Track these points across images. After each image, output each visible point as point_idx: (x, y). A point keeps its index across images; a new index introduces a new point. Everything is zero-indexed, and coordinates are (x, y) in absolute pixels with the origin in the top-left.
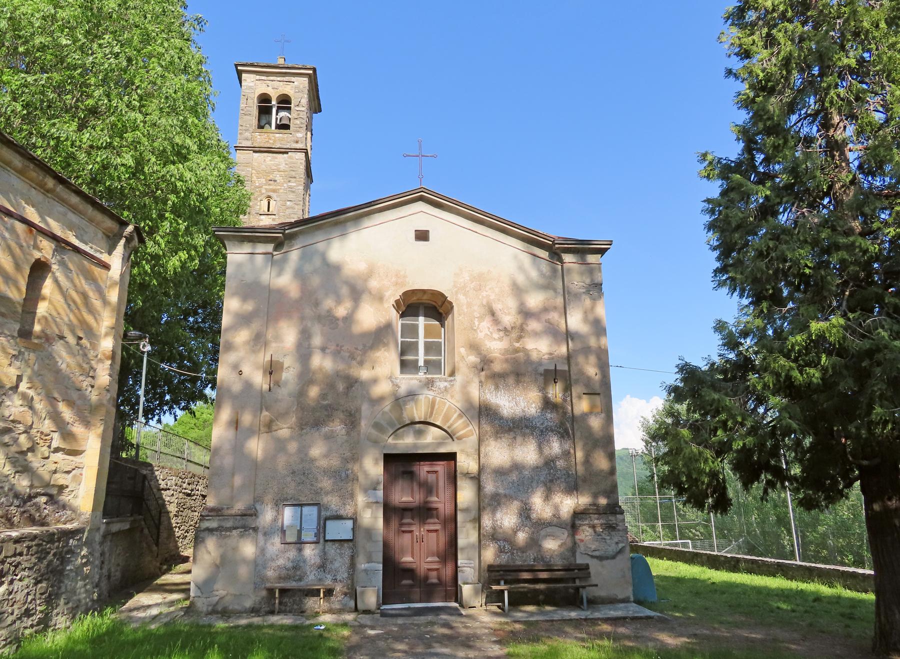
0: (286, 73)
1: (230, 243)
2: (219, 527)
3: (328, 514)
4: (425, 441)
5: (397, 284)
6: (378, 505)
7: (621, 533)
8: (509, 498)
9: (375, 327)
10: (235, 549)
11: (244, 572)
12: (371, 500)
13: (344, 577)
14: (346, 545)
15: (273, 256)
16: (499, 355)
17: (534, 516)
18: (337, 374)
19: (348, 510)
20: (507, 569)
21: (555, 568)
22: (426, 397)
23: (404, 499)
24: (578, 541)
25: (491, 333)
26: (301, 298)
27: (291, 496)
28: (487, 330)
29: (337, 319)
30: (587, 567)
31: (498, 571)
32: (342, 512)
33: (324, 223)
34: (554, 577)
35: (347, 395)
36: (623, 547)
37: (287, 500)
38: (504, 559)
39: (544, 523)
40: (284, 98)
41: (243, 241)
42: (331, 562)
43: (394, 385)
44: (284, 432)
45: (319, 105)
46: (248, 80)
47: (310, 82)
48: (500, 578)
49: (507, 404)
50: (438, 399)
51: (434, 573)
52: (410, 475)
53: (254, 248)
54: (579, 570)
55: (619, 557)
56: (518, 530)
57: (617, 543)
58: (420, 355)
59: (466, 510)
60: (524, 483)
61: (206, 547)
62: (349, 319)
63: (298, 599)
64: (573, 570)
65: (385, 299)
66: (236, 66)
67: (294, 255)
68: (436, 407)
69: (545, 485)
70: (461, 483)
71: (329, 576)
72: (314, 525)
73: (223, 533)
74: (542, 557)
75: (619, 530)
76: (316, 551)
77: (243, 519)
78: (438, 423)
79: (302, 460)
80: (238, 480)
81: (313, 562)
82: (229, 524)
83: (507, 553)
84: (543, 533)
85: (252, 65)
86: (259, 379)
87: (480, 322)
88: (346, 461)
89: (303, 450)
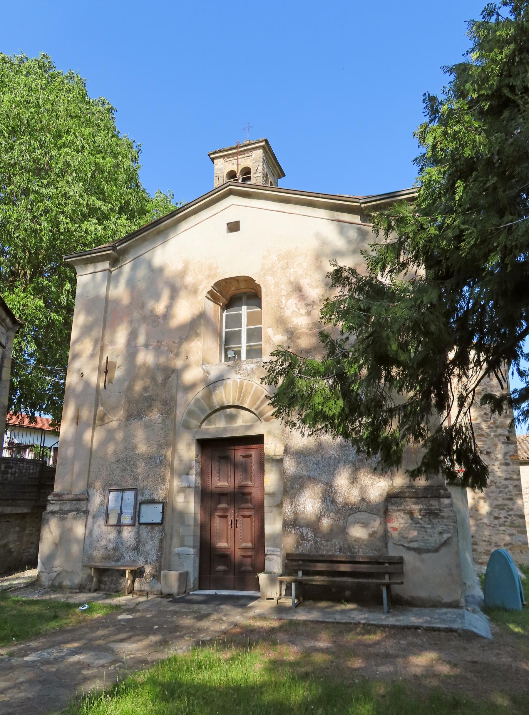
0: (245, 150)
1: (79, 266)
2: (59, 510)
3: (144, 498)
4: (235, 425)
5: (209, 276)
6: (191, 489)
7: (445, 520)
8: (312, 479)
9: (190, 319)
10: (71, 530)
11: (75, 549)
12: (185, 484)
13: (154, 559)
14: (156, 528)
15: (111, 272)
16: (307, 331)
17: (340, 500)
18: (158, 367)
19: (160, 494)
20: (307, 558)
21: (339, 559)
22: (234, 381)
23: (220, 484)
24: (389, 530)
25: (299, 309)
26: (131, 303)
27: (115, 482)
28: (294, 306)
29: (158, 317)
30: (400, 561)
31: (298, 560)
32: (155, 497)
33: (148, 234)
34: (358, 570)
35: (164, 386)
36: (449, 539)
37: (111, 485)
38: (307, 547)
39: (352, 508)
40: (246, 171)
41: (87, 264)
42: (144, 545)
43: (204, 372)
44: (114, 422)
45: (282, 171)
46: (219, 164)
47: (265, 152)
48: (297, 568)
49: (412, 393)
50: (245, 382)
51: (249, 560)
52: (226, 459)
53: (95, 267)
54: (390, 563)
55: (444, 550)
56: (322, 516)
57: (441, 533)
58: (242, 342)
59: (272, 495)
60: (329, 464)
61: (49, 528)
62: (167, 315)
63: (115, 579)
64: (383, 563)
65: (199, 292)
66: (209, 155)
67: (127, 267)
68: (244, 389)
69: (354, 464)
70: (267, 467)
71: (141, 558)
72: (131, 510)
73: (62, 515)
74: (349, 547)
75: (443, 517)
76: (132, 534)
77: (77, 503)
78: (246, 406)
79: (126, 449)
80: (77, 467)
81: (129, 544)
82: (67, 507)
83: (310, 540)
84: (351, 519)
85: (220, 151)
86: (94, 378)
87: (287, 300)
88: (160, 446)
89: (128, 438)
